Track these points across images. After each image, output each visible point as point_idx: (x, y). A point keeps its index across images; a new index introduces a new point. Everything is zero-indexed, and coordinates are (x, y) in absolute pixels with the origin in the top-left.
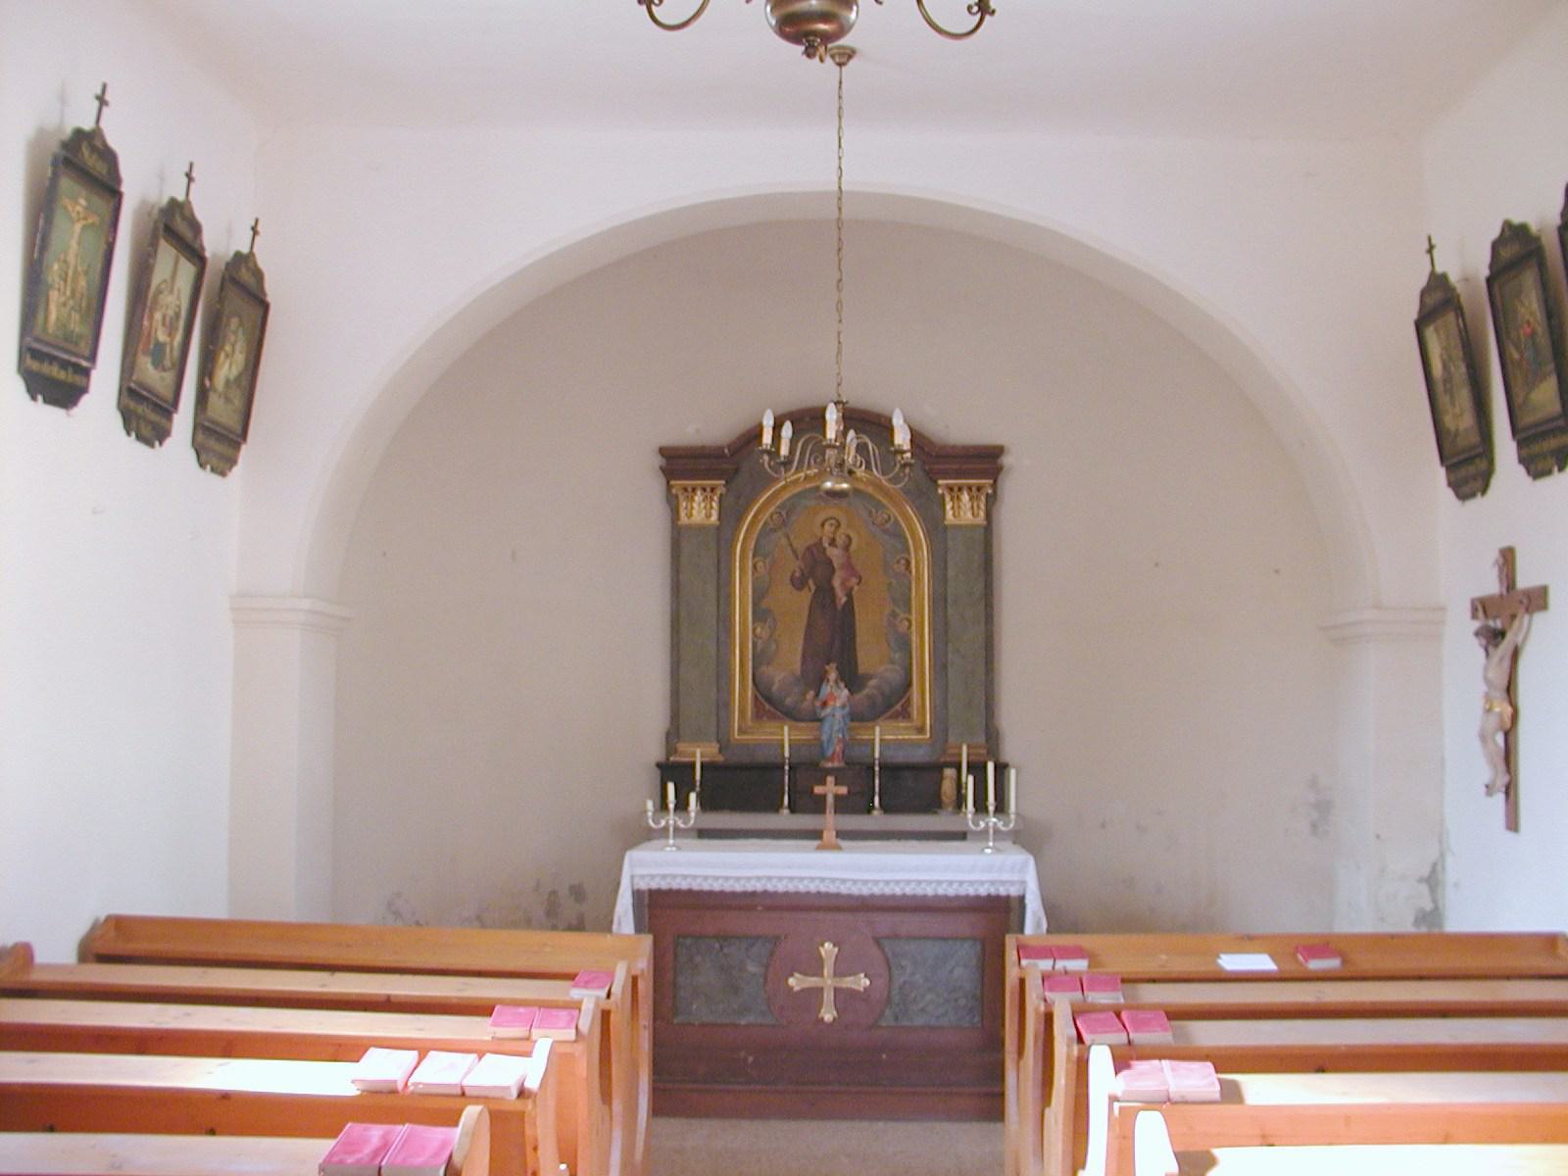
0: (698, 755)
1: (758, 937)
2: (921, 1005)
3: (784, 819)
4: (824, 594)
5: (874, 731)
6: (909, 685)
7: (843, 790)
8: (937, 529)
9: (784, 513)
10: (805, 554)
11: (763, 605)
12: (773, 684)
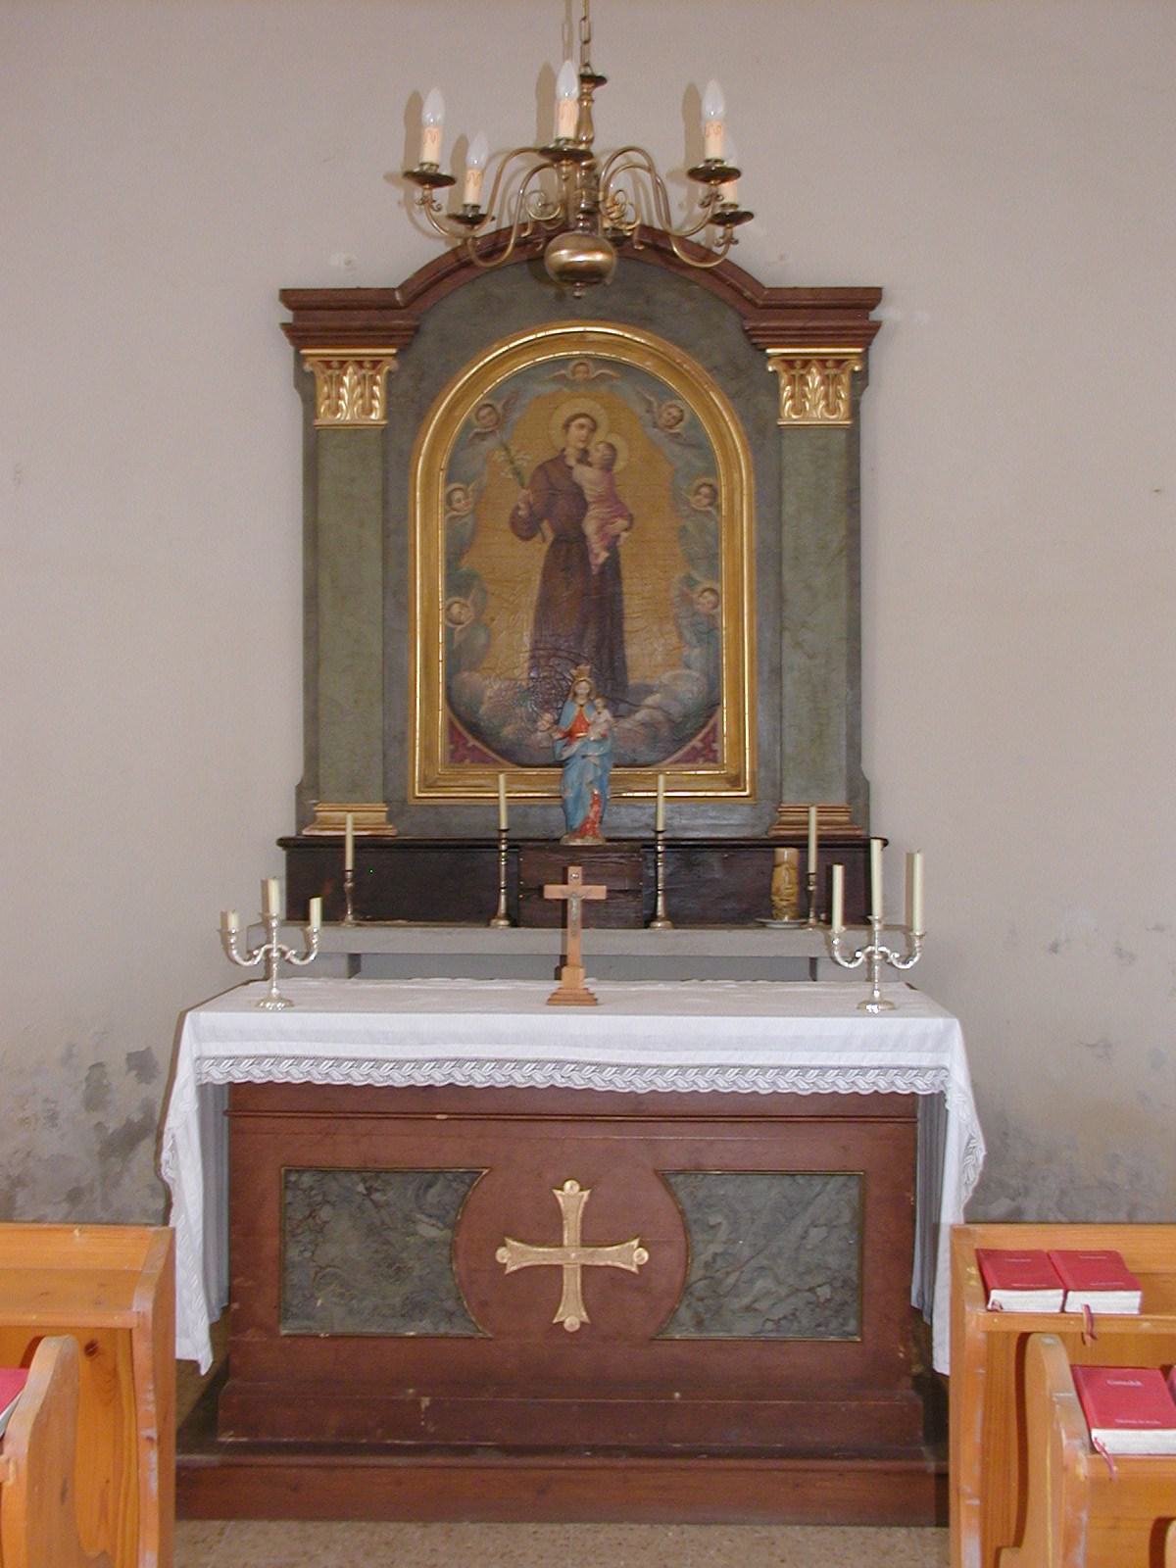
0: (349, 826)
1: (439, 1172)
2: (746, 1301)
3: (498, 937)
4: (569, 548)
5: (657, 783)
6: (712, 706)
7: (598, 892)
8: (764, 432)
9: (499, 407)
10: (534, 477)
11: (465, 565)
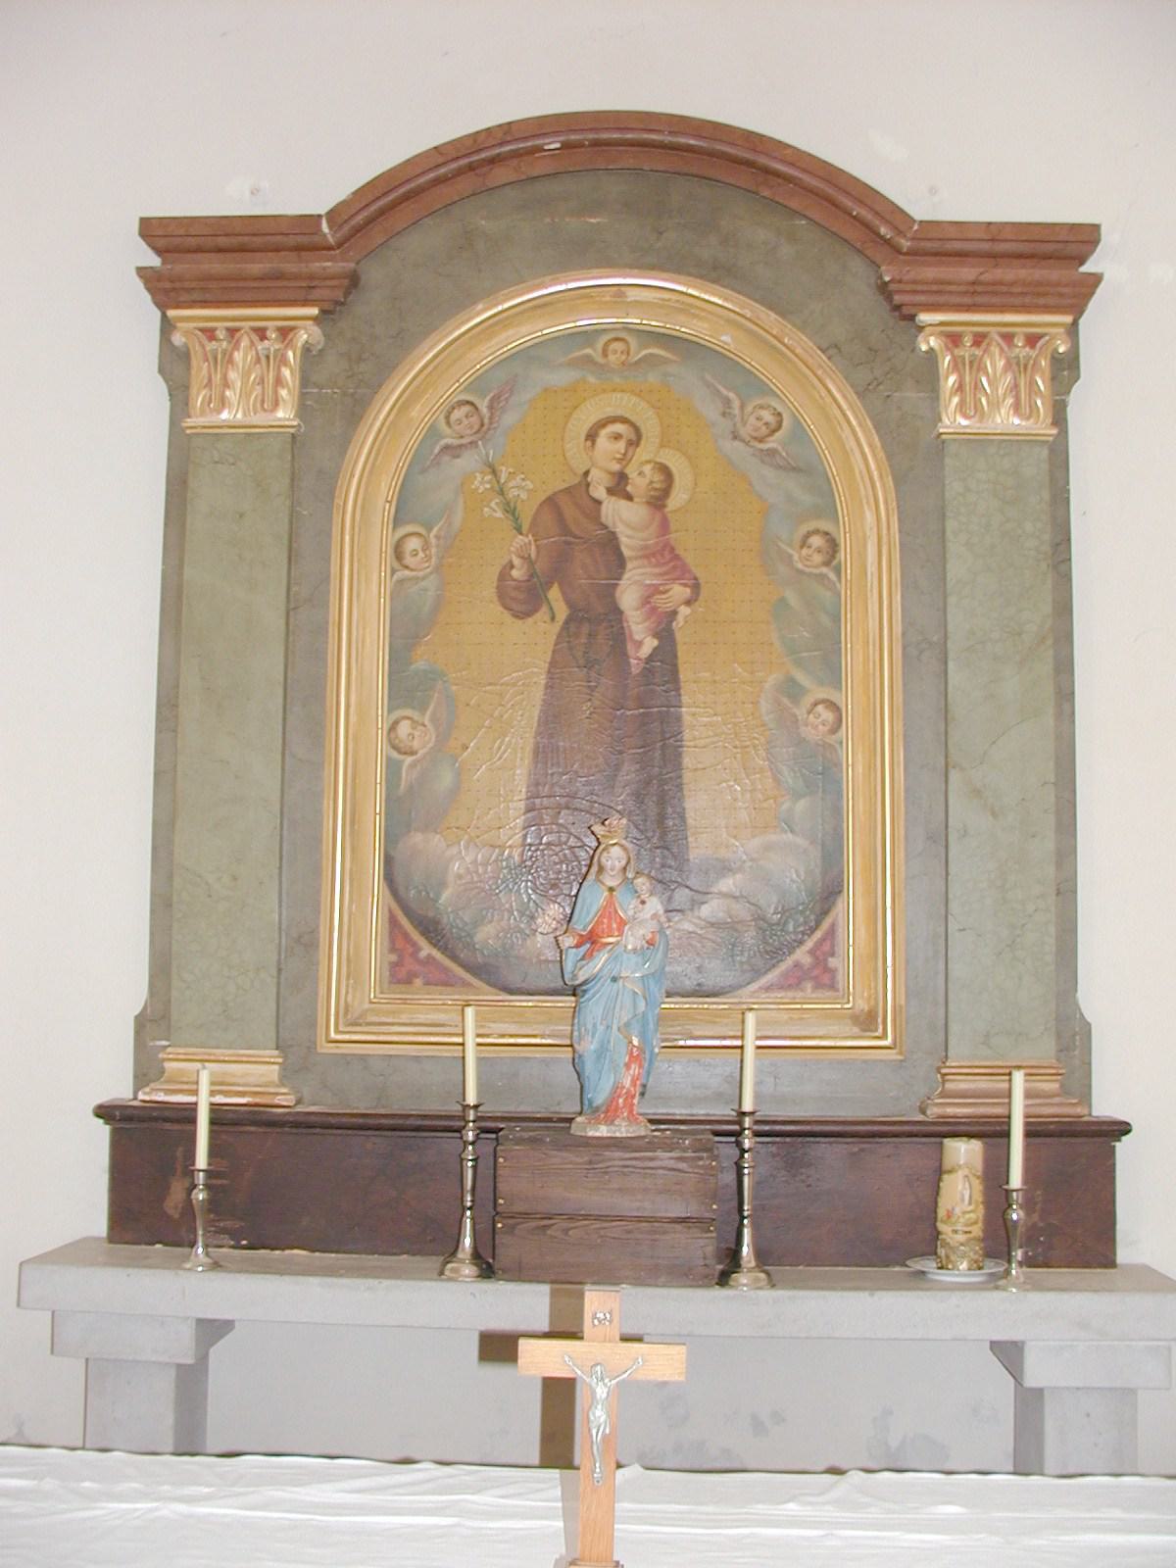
9: (483, 406)
12: (443, 884)
